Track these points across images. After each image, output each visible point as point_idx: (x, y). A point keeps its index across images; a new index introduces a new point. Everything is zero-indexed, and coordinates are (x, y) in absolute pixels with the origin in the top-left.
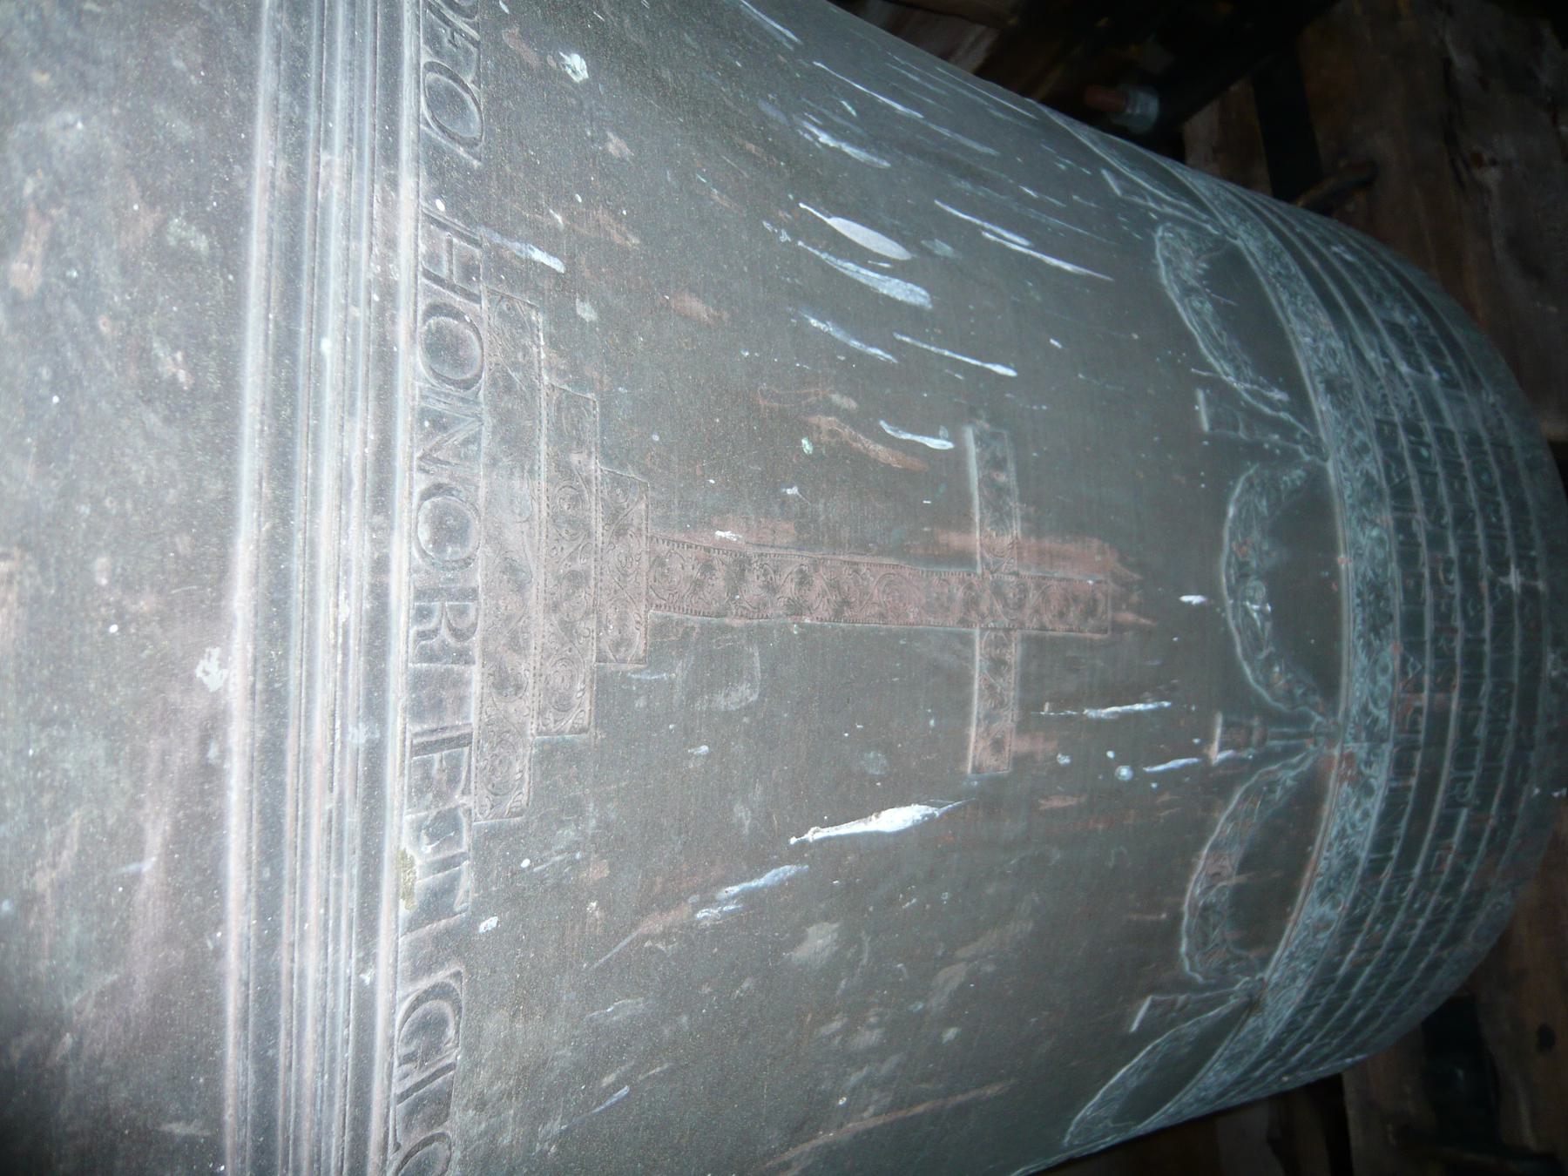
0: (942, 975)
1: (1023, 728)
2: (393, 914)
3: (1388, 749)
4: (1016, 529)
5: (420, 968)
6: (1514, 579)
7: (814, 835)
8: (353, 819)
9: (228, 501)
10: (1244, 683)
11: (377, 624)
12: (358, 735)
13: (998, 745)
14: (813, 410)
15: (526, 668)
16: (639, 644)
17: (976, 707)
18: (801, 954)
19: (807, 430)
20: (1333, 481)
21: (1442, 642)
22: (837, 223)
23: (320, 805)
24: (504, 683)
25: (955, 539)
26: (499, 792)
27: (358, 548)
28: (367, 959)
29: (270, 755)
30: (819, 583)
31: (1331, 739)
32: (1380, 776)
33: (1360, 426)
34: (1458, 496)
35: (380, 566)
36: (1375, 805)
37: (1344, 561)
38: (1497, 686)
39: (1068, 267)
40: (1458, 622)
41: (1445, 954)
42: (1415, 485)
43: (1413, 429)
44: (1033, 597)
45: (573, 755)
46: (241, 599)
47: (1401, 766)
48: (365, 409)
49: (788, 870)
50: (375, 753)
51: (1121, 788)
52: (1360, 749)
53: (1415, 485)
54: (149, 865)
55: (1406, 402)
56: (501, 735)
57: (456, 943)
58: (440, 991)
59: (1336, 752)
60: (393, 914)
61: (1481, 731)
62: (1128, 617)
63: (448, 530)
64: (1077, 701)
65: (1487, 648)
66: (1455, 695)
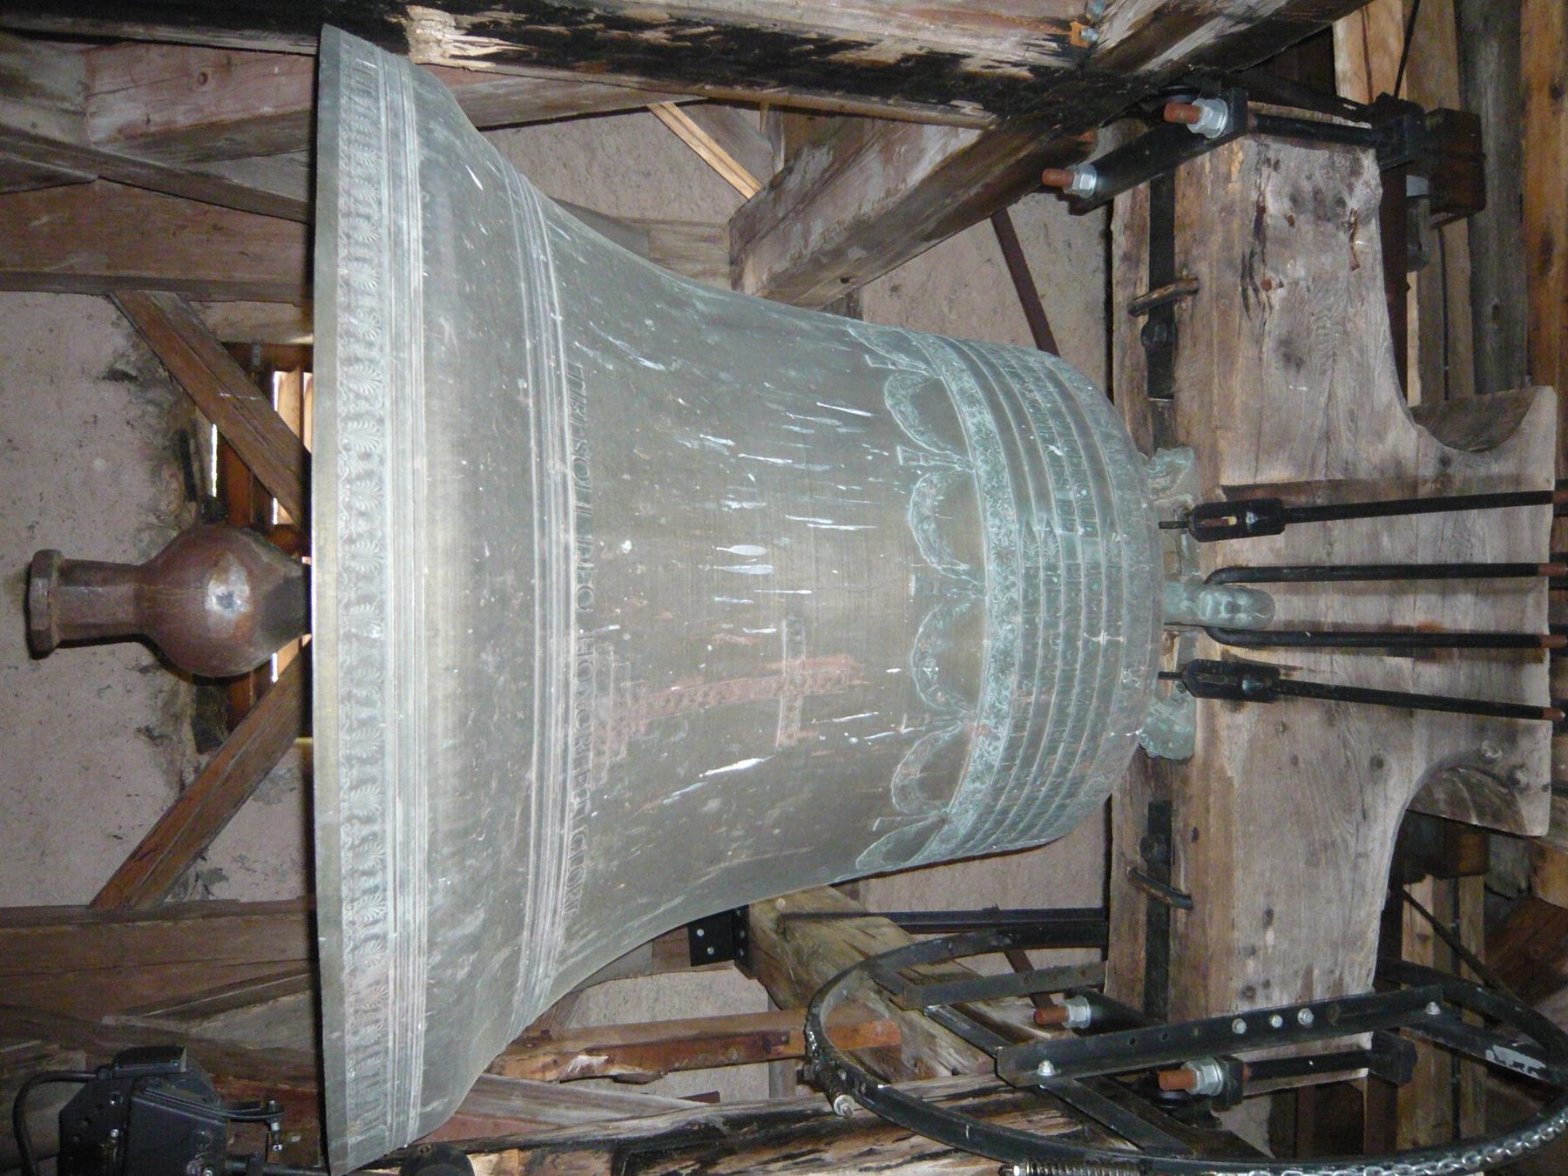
0: (770, 812)
1: (802, 729)
2: (569, 817)
3: (1008, 721)
4: (803, 657)
5: (576, 826)
6: (1103, 638)
7: (709, 773)
8: (559, 798)
9: (532, 738)
10: (921, 701)
11: (565, 751)
12: (560, 778)
13: (790, 736)
14: (713, 633)
15: (606, 748)
16: (643, 729)
17: (781, 723)
18: (706, 809)
19: (709, 642)
20: (987, 605)
21: (1047, 673)
22: (734, 549)
23: (551, 796)
24: (599, 753)
25: (774, 666)
26: (597, 780)
27: (560, 734)
28: (562, 827)
29: (540, 790)
30: (712, 694)
31: (972, 719)
32: (1004, 732)
33: (1013, 573)
34: (1072, 600)
35: (566, 736)
36: (1002, 745)
37: (986, 642)
38: (1083, 690)
39: (851, 528)
40: (1059, 663)
41: (1068, 801)
42: (1043, 599)
43: (1052, 568)
44: (809, 681)
45: (621, 766)
46: (535, 758)
47: (1018, 726)
48: (562, 701)
49: (700, 784)
50: (565, 781)
51: (851, 746)
52: (991, 723)
53: (1043, 599)
54: (517, 818)
55: (1052, 551)
56: (598, 767)
57: (587, 820)
58: (581, 833)
59: (975, 724)
60: (569, 817)
61: (1072, 710)
62: (857, 682)
63: (584, 720)
64: (830, 716)
65: (1078, 673)
66: (1054, 696)
